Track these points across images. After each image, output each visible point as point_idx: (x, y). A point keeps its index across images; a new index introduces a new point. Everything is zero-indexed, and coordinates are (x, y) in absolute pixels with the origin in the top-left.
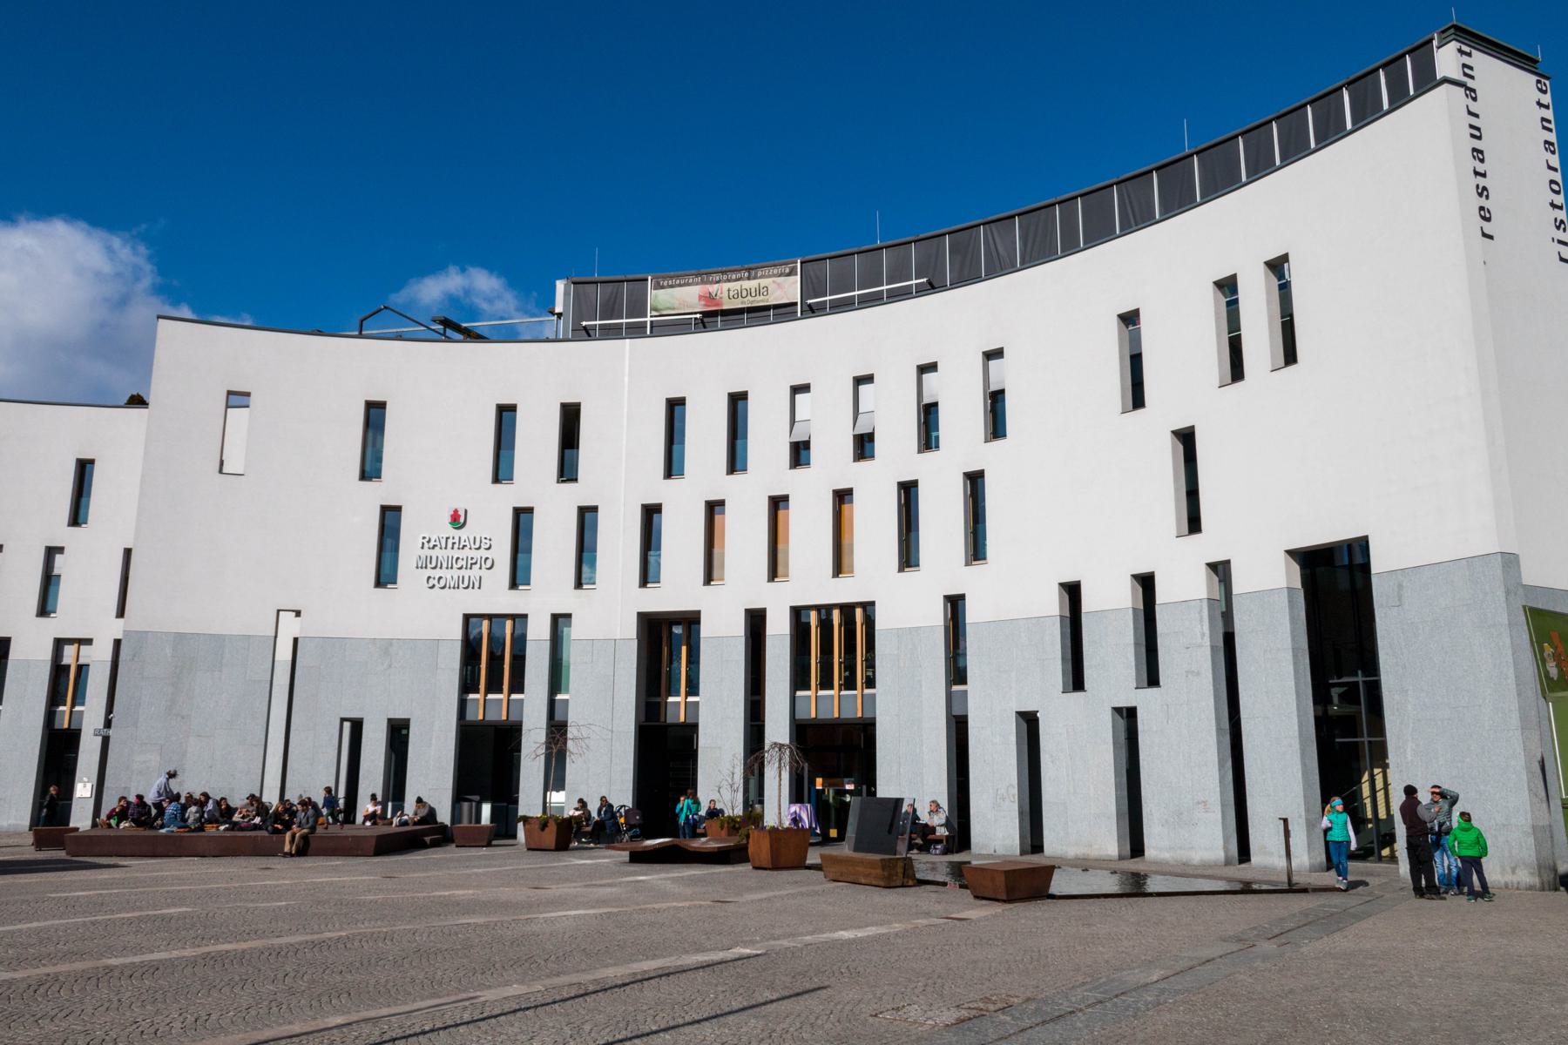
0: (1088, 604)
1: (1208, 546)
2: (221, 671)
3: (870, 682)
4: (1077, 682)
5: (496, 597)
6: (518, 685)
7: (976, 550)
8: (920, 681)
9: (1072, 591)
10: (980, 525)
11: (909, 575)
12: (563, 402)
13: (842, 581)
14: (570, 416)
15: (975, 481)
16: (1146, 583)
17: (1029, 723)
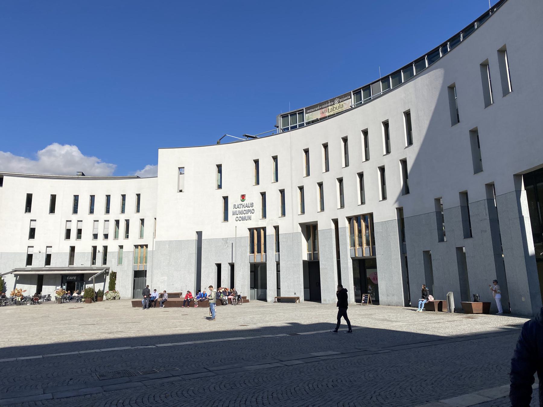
2: (181, 251)
5: (256, 222)
8: (390, 241)
10: (363, 191)
16: (464, 195)
17: (427, 255)
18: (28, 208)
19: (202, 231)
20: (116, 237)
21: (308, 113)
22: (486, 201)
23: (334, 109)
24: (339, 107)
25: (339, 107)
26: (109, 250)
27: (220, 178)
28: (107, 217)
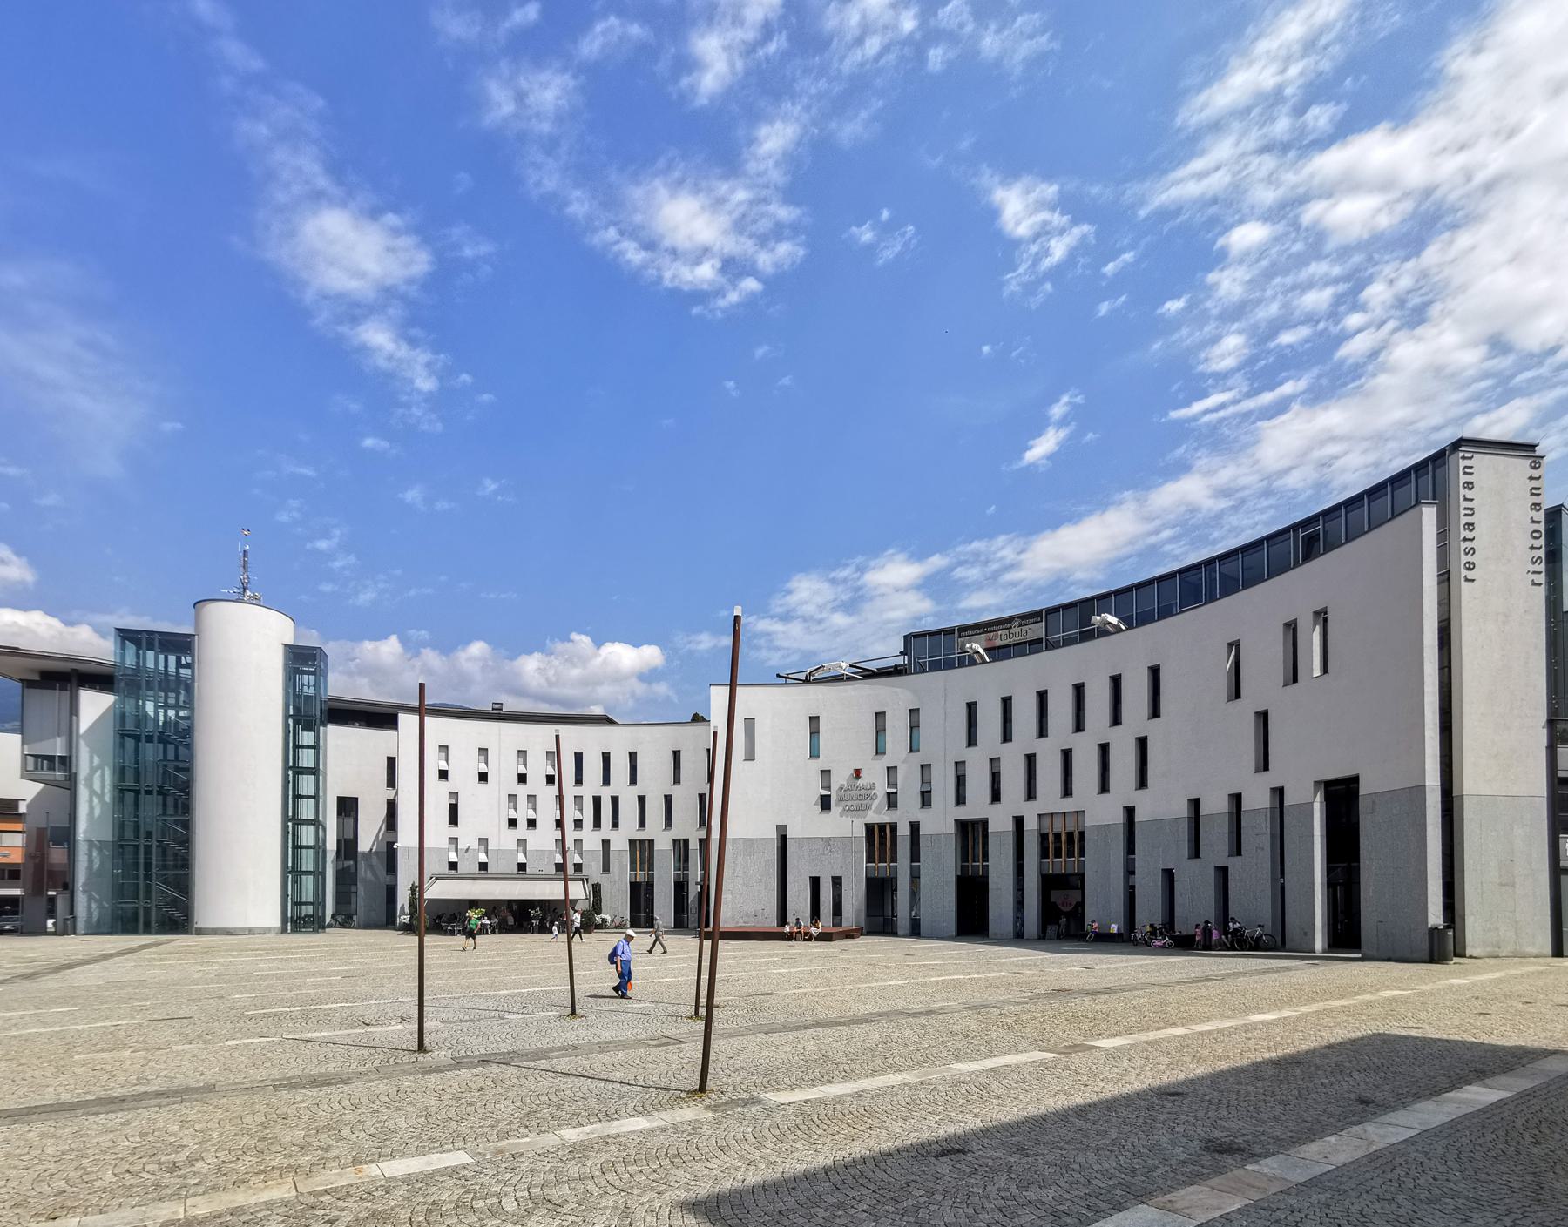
0: (1204, 811)
1: (1272, 779)
3: (1082, 853)
4: (1196, 852)
6: (894, 859)
7: (1142, 783)
9: (1195, 804)
11: (1105, 796)
12: (386, 785)
13: (1068, 800)
14: (633, 756)
15: (1142, 743)
16: (1237, 799)
17: (1169, 875)
20: (597, 824)
21: (963, 637)
22: (1269, 810)
28: (578, 791)
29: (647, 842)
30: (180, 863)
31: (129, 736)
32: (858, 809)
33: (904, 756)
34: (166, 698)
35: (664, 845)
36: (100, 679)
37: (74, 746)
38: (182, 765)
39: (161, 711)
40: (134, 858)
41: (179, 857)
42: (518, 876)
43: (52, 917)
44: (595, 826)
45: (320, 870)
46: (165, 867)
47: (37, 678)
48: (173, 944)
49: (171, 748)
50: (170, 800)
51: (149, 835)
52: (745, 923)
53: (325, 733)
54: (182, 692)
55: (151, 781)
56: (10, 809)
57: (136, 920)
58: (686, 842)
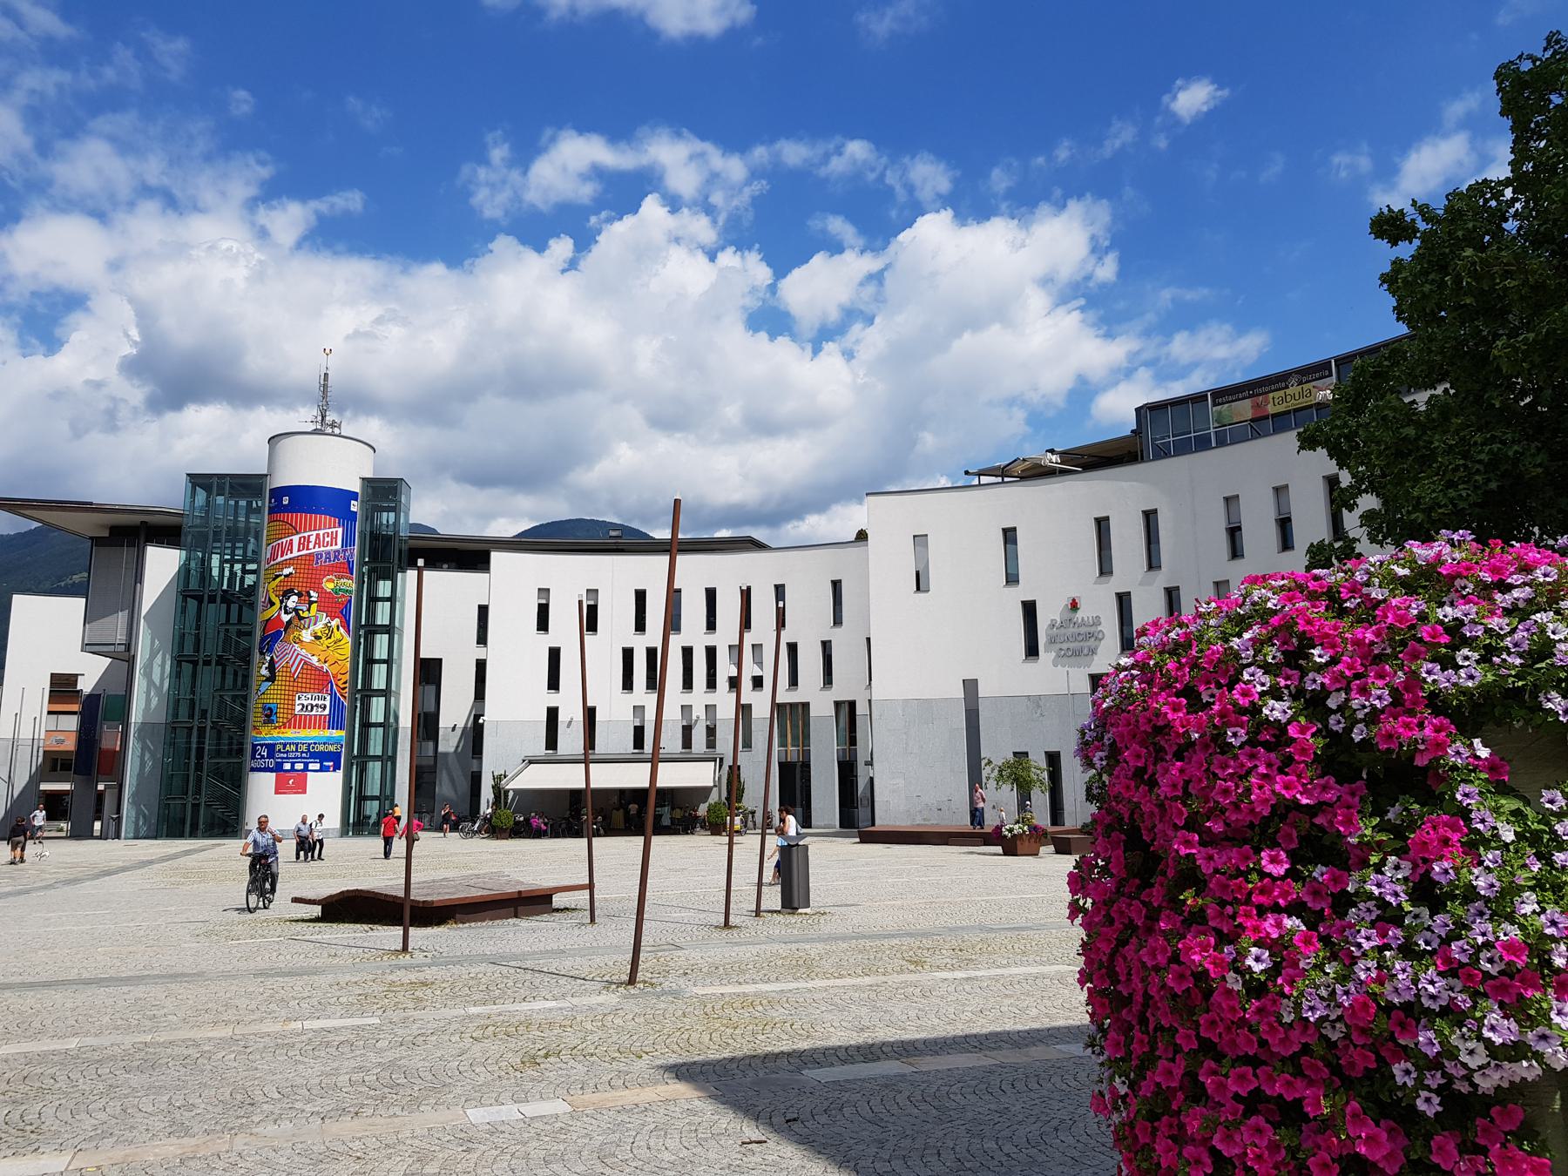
18: (543, 624)
19: (441, 660)
21: (1219, 404)
23: (1289, 397)
24: (1302, 395)
25: (1302, 395)
26: (600, 717)
27: (1153, 559)
29: (788, 707)
30: (235, 747)
31: (192, 597)
32: (1077, 653)
33: (1140, 577)
34: (233, 548)
35: (822, 707)
36: (165, 532)
37: (137, 597)
38: (244, 628)
39: (227, 566)
40: (186, 743)
41: (235, 741)
42: (632, 756)
43: (98, 819)
44: (708, 687)
45: (390, 754)
46: (218, 753)
47: (106, 534)
48: (218, 849)
49: (234, 608)
50: (229, 670)
51: (204, 713)
52: (924, 819)
53: (404, 581)
54: (252, 540)
55: (211, 649)
56: (68, 685)
57: (183, 821)
58: (852, 705)
